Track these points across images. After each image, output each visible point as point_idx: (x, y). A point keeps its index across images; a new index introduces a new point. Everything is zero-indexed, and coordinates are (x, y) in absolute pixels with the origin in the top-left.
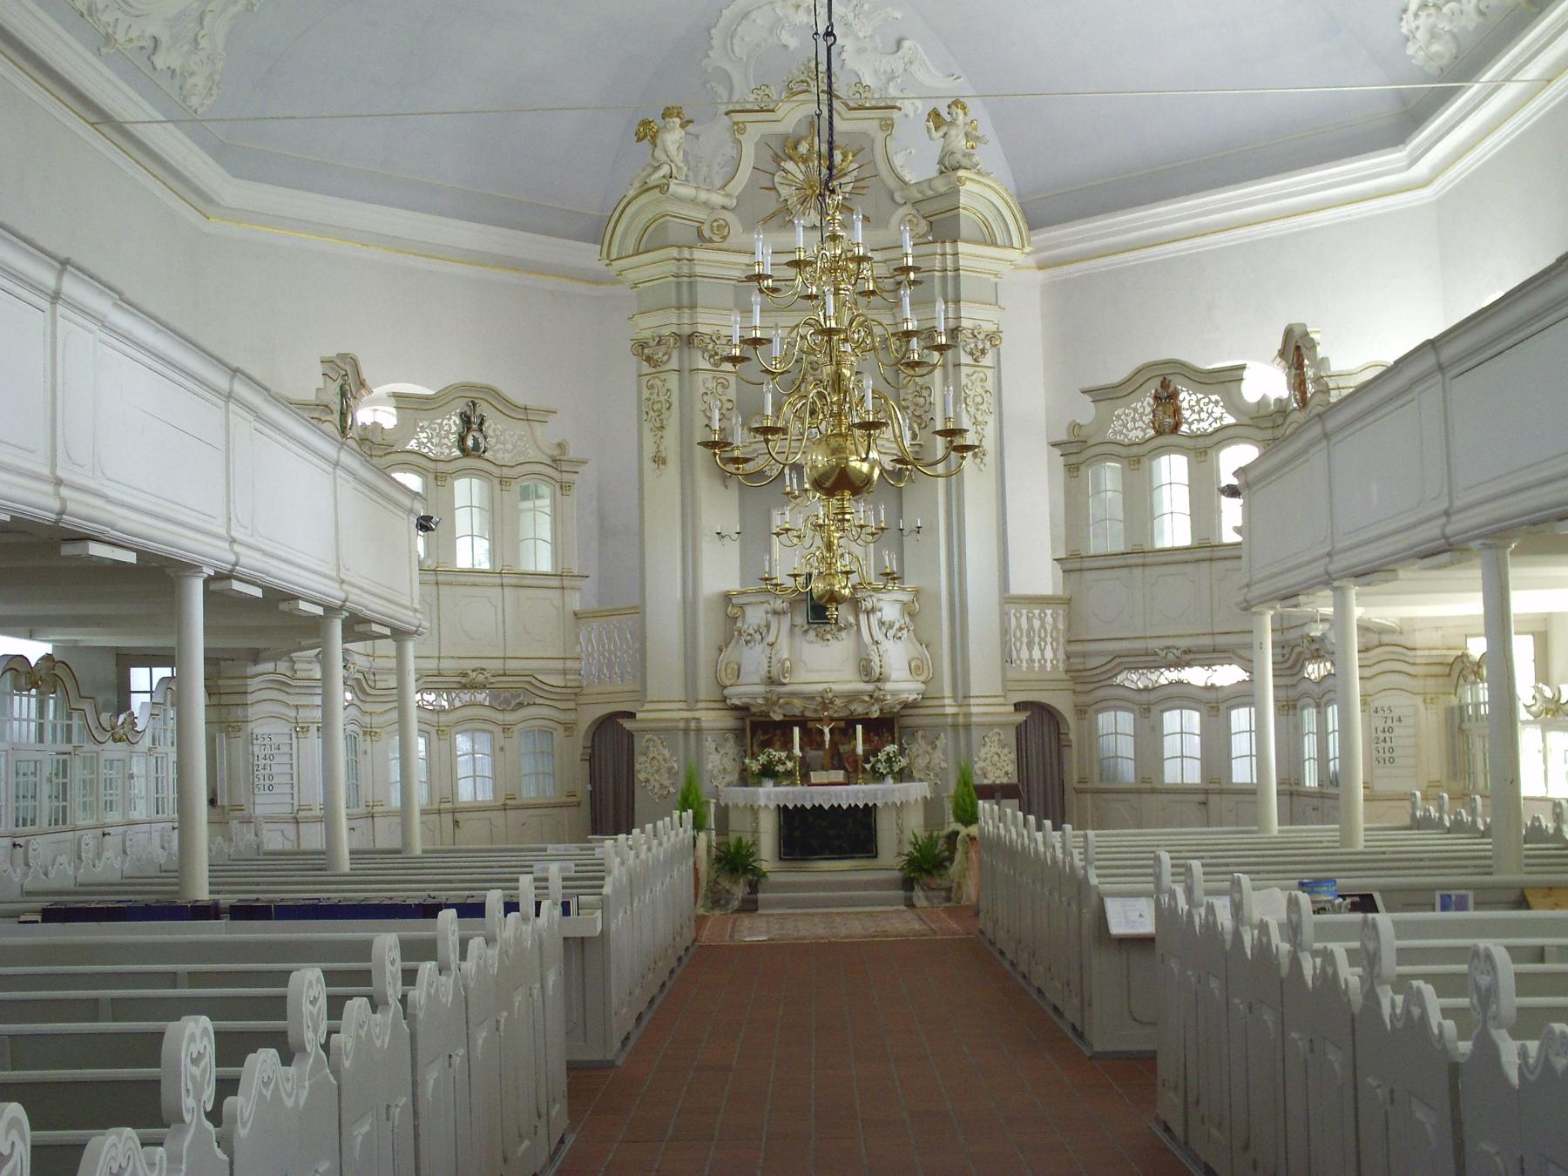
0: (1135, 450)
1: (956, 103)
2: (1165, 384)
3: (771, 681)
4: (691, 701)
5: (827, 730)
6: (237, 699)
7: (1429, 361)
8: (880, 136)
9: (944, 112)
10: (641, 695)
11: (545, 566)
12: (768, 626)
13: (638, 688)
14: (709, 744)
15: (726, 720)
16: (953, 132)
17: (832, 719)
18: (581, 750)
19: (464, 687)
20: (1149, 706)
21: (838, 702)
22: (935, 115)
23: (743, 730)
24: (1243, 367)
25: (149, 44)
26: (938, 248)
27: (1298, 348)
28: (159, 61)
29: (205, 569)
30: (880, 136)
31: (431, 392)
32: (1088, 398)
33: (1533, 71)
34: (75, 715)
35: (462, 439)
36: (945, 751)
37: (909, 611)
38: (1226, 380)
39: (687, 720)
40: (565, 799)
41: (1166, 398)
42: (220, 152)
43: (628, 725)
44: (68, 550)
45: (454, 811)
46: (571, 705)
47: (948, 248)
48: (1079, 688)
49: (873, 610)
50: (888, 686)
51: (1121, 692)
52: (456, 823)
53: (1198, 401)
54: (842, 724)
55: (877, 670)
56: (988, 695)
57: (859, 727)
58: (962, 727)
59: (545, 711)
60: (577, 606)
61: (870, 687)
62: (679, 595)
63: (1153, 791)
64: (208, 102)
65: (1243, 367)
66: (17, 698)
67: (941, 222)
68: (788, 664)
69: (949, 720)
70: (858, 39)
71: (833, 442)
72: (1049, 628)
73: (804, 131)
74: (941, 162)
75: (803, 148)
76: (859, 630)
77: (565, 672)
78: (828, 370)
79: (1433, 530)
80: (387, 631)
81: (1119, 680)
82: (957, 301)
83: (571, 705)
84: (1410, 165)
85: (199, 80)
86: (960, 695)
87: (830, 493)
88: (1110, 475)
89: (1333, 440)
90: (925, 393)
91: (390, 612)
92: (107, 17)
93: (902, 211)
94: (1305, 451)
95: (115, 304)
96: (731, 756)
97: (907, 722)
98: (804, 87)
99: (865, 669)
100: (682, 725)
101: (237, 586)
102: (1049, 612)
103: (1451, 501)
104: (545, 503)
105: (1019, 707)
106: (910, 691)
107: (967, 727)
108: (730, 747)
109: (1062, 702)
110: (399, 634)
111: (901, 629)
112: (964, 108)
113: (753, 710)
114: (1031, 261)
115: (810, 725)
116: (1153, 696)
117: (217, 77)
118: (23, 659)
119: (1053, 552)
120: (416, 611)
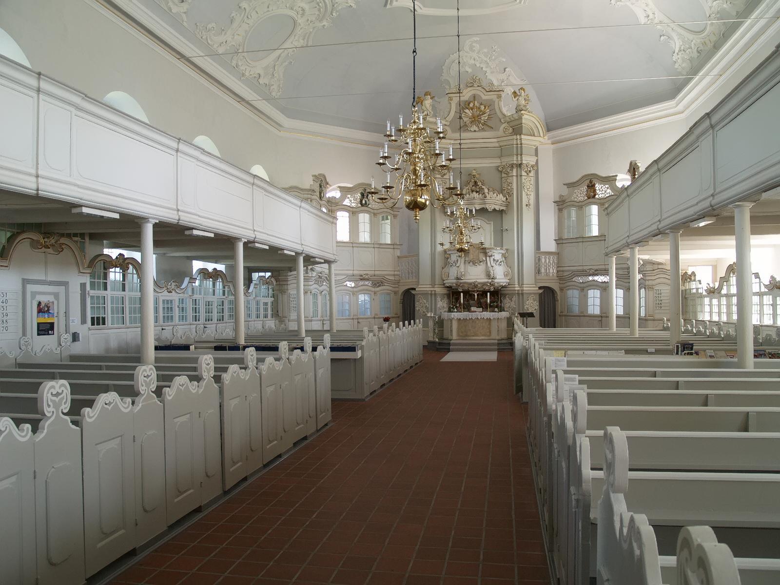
0: (580, 204)
1: (521, 88)
2: (591, 182)
3: (458, 279)
4: (433, 285)
5: (476, 295)
6: (285, 283)
7: (655, 168)
8: (497, 101)
9: (517, 92)
10: (418, 283)
11: (389, 242)
12: (457, 261)
13: (417, 280)
14: (439, 299)
15: (445, 291)
16: (520, 98)
17: (478, 291)
18: (399, 300)
19: (361, 279)
20: (584, 289)
21: (479, 285)
22: (515, 93)
23: (450, 294)
24: (617, 176)
25: (257, 76)
26: (515, 137)
27: (634, 169)
28: (261, 81)
29: (243, 239)
30: (497, 101)
31: (351, 186)
32: (566, 187)
33: (716, 71)
34: (226, 287)
35: (361, 201)
36: (515, 302)
37: (503, 255)
38: (610, 180)
39: (432, 291)
40: (394, 316)
41: (591, 187)
42: (284, 111)
43: (413, 292)
44: (187, 233)
45: (358, 319)
46: (397, 286)
47: (518, 137)
48: (561, 282)
49: (491, 256)
50: (496, 281)
51: (576, 284)
52: (358, 322)
53: (602, 187)
54: (481, 293)
55: (492, 275)
56: (530, 285)
57: (489, 294)
58: (521, 294)
59: (388, 288)
60: (399, 254)
61: (490, 281)
62: (430, 250)
63: (584, 316)
64: (279, 94)
65: (617, 176)
66: (205, 282)
67: (517, 129)
68: (463, 273)
69: (516, 292)
70: (491, 68)
71: (413, 192)
72: (551, 262)
73: (472, 100)
74: (516, 109)
75: (471, 105)
76: (487, 262)
77: (394, 275)
78: (412, 168)
79: (654, 227)
80: (323, 261)
81: (574, 280)
82: (521, 155)
83: (397, 286)
84: (677, 105)
85: (275, 87)
86: (520, 284)
87: (412, 209)
88: (573, 212)
89: (631, 197)
90: (511, 185)
91: (322, 255)
92: (243, 68)
93: (504, 125)
94: (622, 202)
95: (202, 153)
96: (446, 302)
97: (503, 292)
98: (471, 85)
99: (488, 275)
100: (430, 292)
101: (257, 245)
102: (551, 257)
103: (661, 216)
104: (389, 221)
105: (540, 288)
106: (503, 283)
107: (522, 294)
108: (446, 301)
109: (555, 286)
110: (327, 262)
111: (501, 262)
112: (524, 90)
113: (453, 288)
114: (550, 142)
115: (471, 293)
116: (585, 285)
117: (281, 86)
118: (206, 269)
119: (554, 237)
120: (334, 255)
